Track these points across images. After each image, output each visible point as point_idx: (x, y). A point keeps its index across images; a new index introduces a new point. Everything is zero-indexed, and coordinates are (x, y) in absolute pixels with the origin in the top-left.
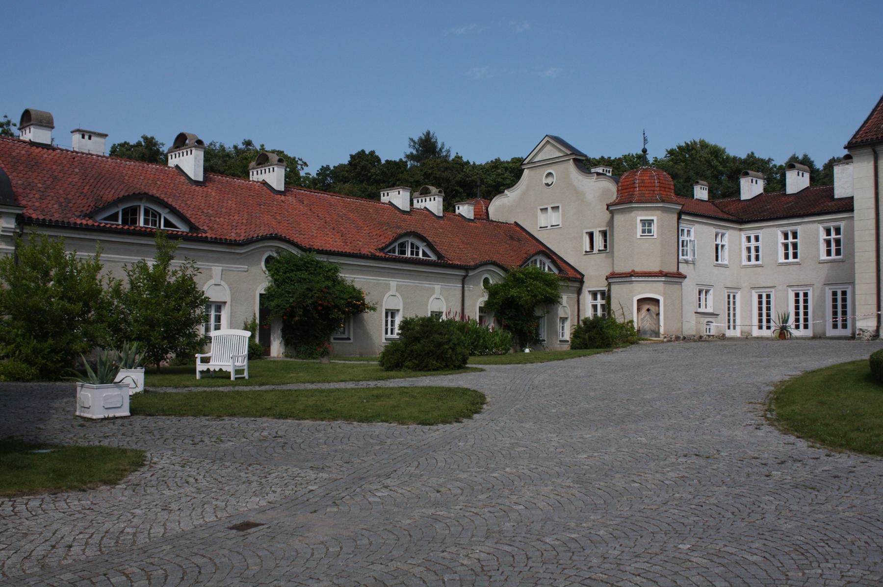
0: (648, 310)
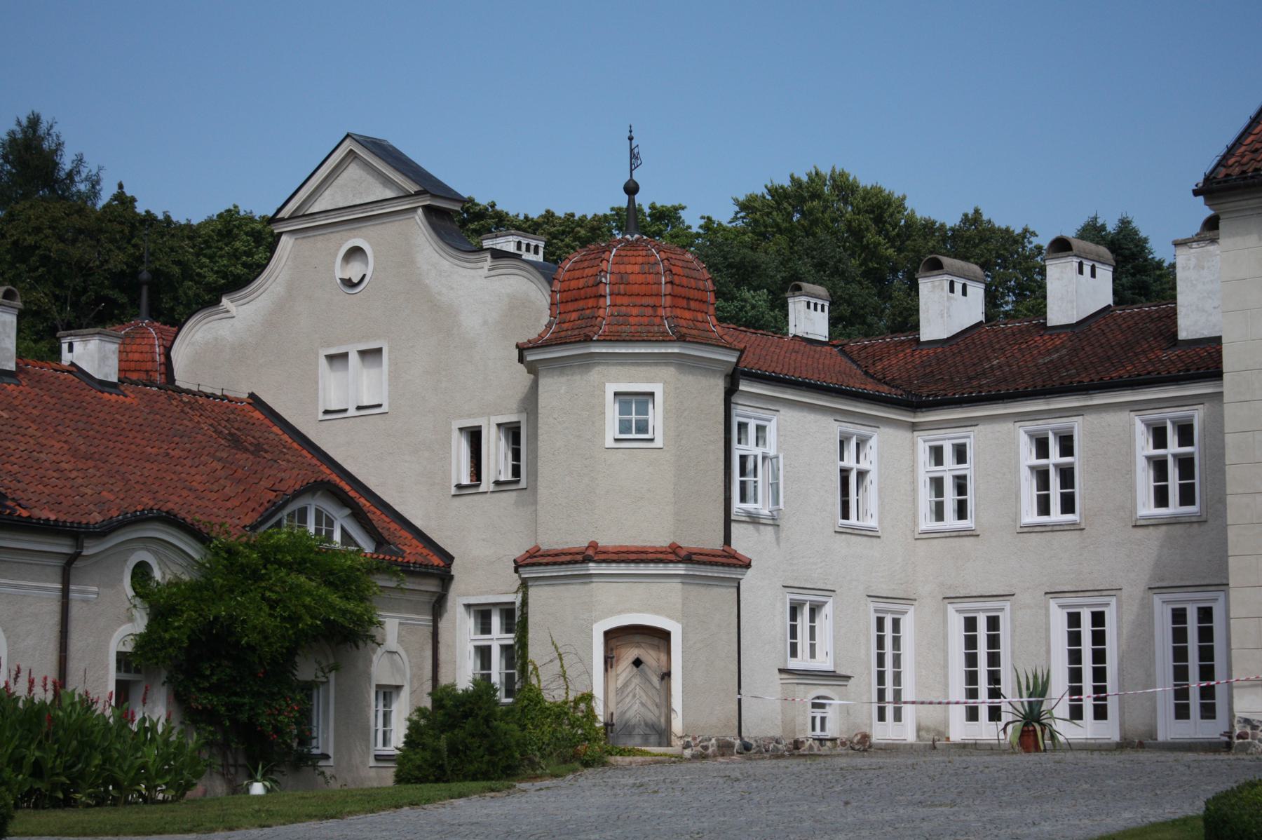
0: (637, 663)
